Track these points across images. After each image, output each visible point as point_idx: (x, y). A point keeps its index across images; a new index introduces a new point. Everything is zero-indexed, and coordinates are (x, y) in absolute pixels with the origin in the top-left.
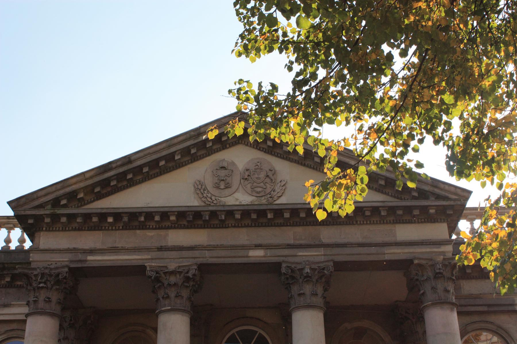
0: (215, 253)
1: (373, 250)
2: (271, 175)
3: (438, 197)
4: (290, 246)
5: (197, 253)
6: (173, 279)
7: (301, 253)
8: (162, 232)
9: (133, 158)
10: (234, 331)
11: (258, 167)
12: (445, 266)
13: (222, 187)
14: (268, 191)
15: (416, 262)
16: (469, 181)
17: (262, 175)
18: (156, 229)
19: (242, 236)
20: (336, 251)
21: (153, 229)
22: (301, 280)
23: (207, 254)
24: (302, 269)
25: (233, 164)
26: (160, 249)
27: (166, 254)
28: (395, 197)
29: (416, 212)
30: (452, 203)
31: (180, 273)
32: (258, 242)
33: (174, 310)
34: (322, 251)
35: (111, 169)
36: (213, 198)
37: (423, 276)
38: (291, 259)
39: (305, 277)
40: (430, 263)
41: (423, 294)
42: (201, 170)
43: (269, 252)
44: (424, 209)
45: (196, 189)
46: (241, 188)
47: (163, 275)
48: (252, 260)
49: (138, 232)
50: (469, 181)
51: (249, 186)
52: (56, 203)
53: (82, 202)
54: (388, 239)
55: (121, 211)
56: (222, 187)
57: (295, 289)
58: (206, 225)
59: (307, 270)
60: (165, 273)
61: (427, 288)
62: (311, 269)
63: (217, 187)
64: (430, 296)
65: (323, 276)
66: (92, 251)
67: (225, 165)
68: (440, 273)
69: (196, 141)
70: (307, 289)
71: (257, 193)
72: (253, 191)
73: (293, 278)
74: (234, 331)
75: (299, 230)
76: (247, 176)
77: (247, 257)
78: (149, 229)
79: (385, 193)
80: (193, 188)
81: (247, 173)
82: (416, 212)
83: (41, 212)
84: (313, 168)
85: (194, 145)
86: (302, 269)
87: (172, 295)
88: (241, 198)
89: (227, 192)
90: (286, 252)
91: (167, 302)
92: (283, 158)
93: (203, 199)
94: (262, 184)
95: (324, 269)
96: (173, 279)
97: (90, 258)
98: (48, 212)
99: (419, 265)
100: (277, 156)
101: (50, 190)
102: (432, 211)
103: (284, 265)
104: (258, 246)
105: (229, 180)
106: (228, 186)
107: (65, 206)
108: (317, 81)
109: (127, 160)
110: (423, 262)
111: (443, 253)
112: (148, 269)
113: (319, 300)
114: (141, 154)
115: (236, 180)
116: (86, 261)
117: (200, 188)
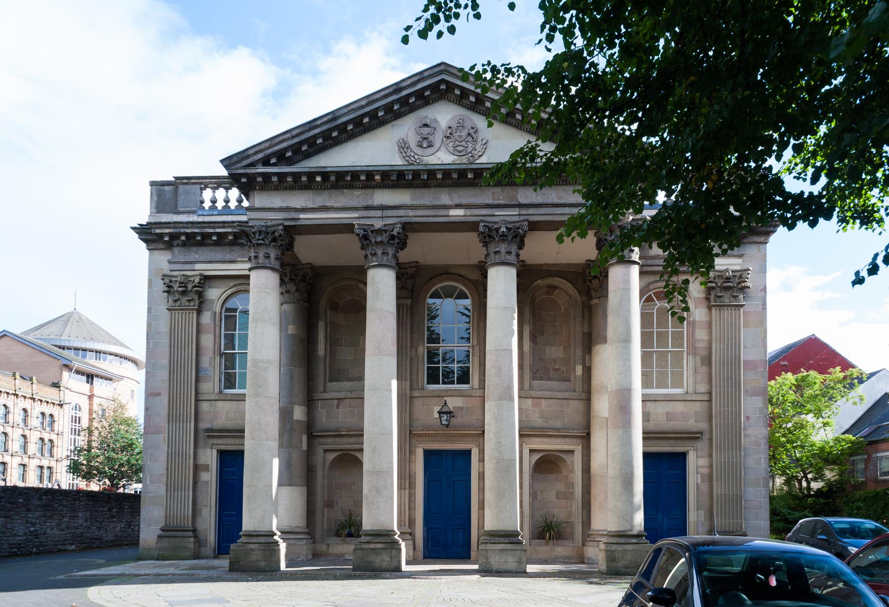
14: (469, 149)
19: (445, 197)
20: (531, 211)
21: (359, 188)
23: (411, 213)
24: (500, 228)
25: (436, 121)
26: (367, 208)
34: (515, 212)
36: (416, 157)
42: (405, 129)
43: (469, 212)
45: (400, 147)
46: (443, 148)
51: (451, 144)
56: (425, 145)
60: (372, 231)
62: (507, 228)
63: (420, 146)
66: (304, 210)
67: (428, 122)
71: (460, 152)
72: (455, 151)
73: (490, 236)
81: (449, 131)
84: (515, 126)
87: (379, 252)
88: (442, 157)
97: (302, 216)
104: (458, 206)
105: (431, 138)
106: (430, 146)
107: (274, 165)
112: (356, 227)
115: (438, 139)
117: (403, 146)
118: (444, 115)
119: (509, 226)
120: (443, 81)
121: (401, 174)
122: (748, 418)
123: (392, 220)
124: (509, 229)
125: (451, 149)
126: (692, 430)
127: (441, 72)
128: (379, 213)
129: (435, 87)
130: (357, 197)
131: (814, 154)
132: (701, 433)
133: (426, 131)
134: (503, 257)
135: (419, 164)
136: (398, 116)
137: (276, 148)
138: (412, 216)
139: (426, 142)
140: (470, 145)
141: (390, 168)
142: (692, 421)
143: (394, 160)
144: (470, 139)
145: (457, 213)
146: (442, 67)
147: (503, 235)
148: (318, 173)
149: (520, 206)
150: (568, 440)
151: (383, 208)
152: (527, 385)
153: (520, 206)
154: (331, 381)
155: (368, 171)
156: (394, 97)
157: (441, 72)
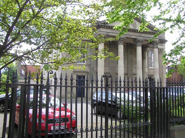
7: (139, 37)
19: (131, 33)
34: (142, 37)
104: (134, 35)
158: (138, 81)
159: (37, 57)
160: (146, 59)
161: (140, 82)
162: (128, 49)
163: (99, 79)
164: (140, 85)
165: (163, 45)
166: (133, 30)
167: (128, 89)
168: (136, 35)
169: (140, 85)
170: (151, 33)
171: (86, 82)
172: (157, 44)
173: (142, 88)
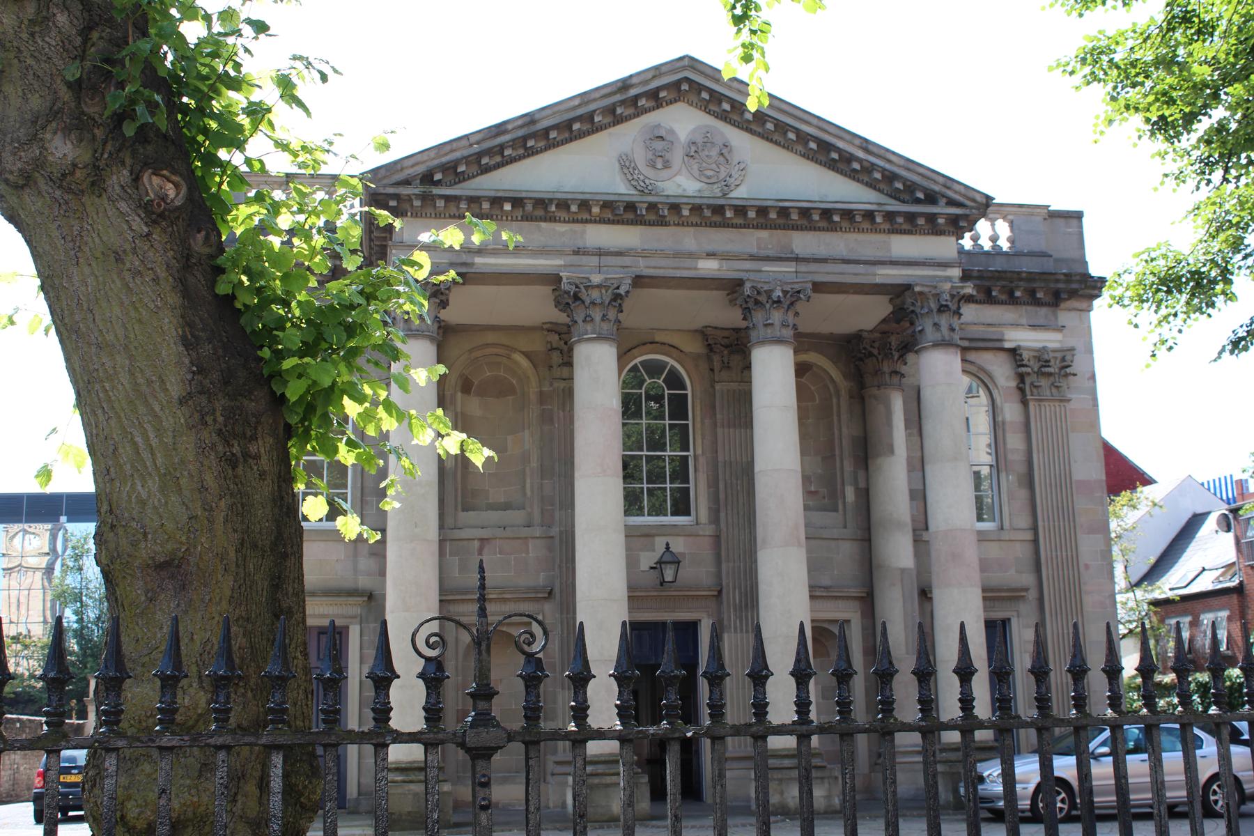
0: (652, 262)
1: (861, 268)
2: (725, 151)
3: (951, 203)
4: (753, 258)
5: (627, 261)
6: (595, 294)
7: (768, 267)
8: (577, 227)
9: (537, 116)
10: (672, 362)
11: (708, 142)
12: (953, 296)
13: (659, 166)
14: (722, 175)
15: (917, 289)
16: (1076, 217)
17: (714, 153)
18: (568, 222)
19: (689, 239)
20: (813, 267)
21: (565, 222)
22: (768, 306)
23: (642, 262)
24: (772, 291)
25: (672, 132)
26: (577, 252)
27: (584, 260)
28: (891, 196)
29: (921, 221)
30: (967, 212)
31: (607, 288)
32: (710, 248)
33: (601, 338)
34: (790, 268)
35: (505, 132)
36: (647, 182)
37: (922, 308)
38: (752, 276)
39: (774, 302)
40: (934, 292)
41: (920, 331)
42: (626, 138)
43: (725, 265)
44: (931, 218)
45: (622, 167)
46: (684, 170)
47: (583, 290)
48: (701, 274)
49: (543, 225)
50: (1076, 217)
51: (696, 167)
52: (427, 178)
53: (461, 178)
54: (880, 254)
55: (524, 195)
56: (659, 166)
57: (758, 317)
58: (639, 221)
59: (778, 293)
60: (587, 288)
61: (926, 324)
62: (783, 291)
63: (652, 165)
64: (931, 335)
65: (792, 298)
67: (663, 133)
68: (947, 306)
69: (624, 97)
70: (777, 316)
71: (709, 178)
72: (701, 175)
73: (757, 302)
74: (672, 362)
75: (764, 234)
76: (694, 151)
77: (696, 269)
78: (560, 221)
79: (879, 190)
80: (617, 165)
81: (693, 148)
82: (921, 221)
83: (404, 191)
84: (784, 147)
85: (623, 102)
86: (772, 291)
87: (598, 318)
88: (683, 184)
89: (665, 173)
90: (748, 265)
91: (589, 327)
92: (742, 129)
93: (634, 183)
94: (714, 166)
95: (799, 292)
96: (595, 294)
98: (416, 191)
99: (921, 293)
100: (734, 125)
101: (419, 158)
102: (941, 221)
103: (748, 285)
104: (711, 255)
105: (668, 156)
106: (667, 165)
108: (1203, 125)
109: (529, 119)
110: (926, 290)
111: (949, 279)
112: (564, 280)
113: (788, 333)
114: (549, 112)
115: (677, 157)
116: (473, 264)
117: (626, 165)
118: (683, 121)
119: (787, 288)
120: (687, 79)
121: (631, 206)
122: (1087, 567)
123: (619, 272)
124: (785, 293)
125: (696, 173)
126: (1014, 585)
127: (684, 68)
128: (594, 260)
129: (676, 85)
130: (560, 233)
131: (105, 143)
132: (1026, 590)
133: (659, 145)
134: (777, 332)
135: (656, 195)
136: (619, 120)
137: (444, 160)
138: (643, 267)
139: (660, 160)
140: (723, 169)
141: (616, 198)
142: (1012, 571)
143: (619, 187)
144: (722, 159)
145: (709, 267)
146: (686, 62)
147: (779, 302)
148: (507, 199)
149: (797, 259)
150: (840, 603)
151: (600, 253)
152: (449, 521)
153: (797, 259)
154: (465, 509)
155: (782, 208)
156: (618, 97)
157: (684, 68)
158: (947, 654)
159: (346, 501)
160: (891, 450)
161: (965, 672)
162: (713, 383)
163: (781, 658)
164: (967, 702)
165: (1064, 317)
166: (696, 209)
167: (1150, 730)
168: (729, 247)
169: (967, 702)
170: (752, 214)
171: (704, 687)
172: (942, 309)
173: (397, 722)
